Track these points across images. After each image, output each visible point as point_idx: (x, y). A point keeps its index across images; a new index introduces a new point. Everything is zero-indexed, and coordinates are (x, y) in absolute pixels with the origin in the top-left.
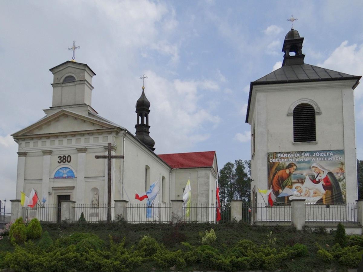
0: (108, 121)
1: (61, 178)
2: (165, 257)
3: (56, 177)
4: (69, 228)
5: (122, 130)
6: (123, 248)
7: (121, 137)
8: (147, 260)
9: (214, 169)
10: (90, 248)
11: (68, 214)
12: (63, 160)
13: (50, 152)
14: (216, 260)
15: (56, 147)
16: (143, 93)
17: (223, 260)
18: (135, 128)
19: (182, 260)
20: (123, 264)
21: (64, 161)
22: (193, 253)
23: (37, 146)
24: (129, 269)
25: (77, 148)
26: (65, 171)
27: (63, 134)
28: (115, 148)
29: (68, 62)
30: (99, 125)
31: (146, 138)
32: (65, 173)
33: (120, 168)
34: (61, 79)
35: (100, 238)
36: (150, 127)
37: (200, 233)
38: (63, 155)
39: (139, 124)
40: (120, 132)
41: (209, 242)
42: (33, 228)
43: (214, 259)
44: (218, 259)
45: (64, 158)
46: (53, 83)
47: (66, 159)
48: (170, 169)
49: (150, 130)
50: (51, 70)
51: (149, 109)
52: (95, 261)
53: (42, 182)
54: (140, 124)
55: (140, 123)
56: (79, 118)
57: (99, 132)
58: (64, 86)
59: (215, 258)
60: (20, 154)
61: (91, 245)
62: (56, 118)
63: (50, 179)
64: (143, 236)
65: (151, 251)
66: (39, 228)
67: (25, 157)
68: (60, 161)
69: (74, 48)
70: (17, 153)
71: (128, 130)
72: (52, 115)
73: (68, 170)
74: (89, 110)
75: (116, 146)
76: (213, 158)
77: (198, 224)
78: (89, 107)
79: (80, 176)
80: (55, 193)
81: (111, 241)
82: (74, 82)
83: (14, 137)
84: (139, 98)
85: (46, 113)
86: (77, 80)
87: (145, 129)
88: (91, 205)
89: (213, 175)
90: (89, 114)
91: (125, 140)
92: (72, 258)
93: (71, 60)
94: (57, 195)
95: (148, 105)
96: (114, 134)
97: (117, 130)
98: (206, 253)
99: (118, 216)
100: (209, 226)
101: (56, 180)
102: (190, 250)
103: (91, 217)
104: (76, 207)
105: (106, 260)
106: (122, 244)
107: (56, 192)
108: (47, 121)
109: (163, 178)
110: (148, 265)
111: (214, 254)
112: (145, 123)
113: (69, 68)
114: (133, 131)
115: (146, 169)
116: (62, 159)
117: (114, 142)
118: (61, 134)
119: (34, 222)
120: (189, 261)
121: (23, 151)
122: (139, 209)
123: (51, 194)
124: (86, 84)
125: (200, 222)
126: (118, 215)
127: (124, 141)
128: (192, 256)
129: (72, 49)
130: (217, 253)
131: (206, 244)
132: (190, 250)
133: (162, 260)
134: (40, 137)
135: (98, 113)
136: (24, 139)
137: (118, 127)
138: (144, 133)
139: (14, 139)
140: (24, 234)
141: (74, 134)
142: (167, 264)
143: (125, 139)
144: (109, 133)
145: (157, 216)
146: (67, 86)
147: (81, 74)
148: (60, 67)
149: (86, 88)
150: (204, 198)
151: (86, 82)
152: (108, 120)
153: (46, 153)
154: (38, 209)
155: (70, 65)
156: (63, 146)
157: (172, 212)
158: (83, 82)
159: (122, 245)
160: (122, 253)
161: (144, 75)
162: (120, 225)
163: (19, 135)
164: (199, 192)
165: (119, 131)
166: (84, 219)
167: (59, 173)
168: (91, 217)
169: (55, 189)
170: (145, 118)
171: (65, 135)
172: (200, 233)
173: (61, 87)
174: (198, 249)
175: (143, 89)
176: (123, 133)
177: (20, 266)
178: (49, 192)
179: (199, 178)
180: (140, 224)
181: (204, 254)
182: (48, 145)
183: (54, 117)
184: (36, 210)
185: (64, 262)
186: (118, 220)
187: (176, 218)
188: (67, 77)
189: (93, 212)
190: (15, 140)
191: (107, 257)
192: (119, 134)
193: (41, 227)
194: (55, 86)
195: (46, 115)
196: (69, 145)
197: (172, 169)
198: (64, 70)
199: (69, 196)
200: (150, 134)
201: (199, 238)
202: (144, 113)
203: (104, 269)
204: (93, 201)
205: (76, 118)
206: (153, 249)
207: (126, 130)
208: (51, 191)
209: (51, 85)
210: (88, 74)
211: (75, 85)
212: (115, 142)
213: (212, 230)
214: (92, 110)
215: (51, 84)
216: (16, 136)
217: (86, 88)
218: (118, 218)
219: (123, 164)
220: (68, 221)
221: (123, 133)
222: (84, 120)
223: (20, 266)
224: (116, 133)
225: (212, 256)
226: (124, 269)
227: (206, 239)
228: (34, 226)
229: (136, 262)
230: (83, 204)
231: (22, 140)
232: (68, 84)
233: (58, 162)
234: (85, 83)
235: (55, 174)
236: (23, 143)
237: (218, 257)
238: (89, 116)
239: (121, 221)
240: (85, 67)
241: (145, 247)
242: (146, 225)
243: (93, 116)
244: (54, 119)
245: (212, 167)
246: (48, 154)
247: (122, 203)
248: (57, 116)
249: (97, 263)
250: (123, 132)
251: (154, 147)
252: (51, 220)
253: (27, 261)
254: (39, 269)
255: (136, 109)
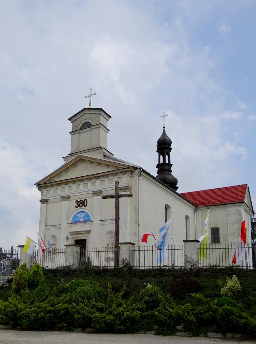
0: (123, 162)
1: (78, 222)
2: (170, 311)
3: (73, 222)
4: (72, 274)
5: (136, 168)
6: (121, 299)
7: (136, 176)
8: (148, 315)
9: (247, 204)
10: (83, 298)
11: (72, 258)
12: (80, 204)
13: (68, 198)
14: (238, 319)
15: (74, 192)
16: (164, 132)
17: (249, 318)
18: (156, 167)
19: (192, 318)
20: (118, 319)
21: (81, 205)
22: (207, 308)
23: (57, 193)
24: (124, 326)
25: (92, 191)
26: (82, 215)
27: (80, 179)
28: (130, 188)
29: (85, 109)
30: (113, 166)
31: (168, 176)
32: (81, 217)
33: (135, 209)
34: (78, 127)
35: (100, 286)
36: (172, 165)
37: (220, 282)
38: (84, 199)
39: (161, 163)
40: (135, 171)
41: (230, 292)
42: (34, 274)
43: (234, 317)
44: (241, 317)
45: (81, 202)
46: (71, 131)
47: (83, 203)
48: (194, 208)
49: (172, 169)
50: (69, 119)
51: (171, 147)
52: (85, 315)
53: (60, 227)
54: (162, 163)
55: (162, 162)
56: (94, 162)
57: (114, 174)
58: (81, 133)
59: (237, 316)
60: (42, 201)
61: (85, 294)
62: (73, 164)
63: (67, 224)
64: (147, 284)
65: (153, 304)
66: (40, 274)
67: (46, 204)
68: (77, 206)
69: (91, 95)
70: (40, 200)
71: (142, 168)
72: (70, 161)
73: (84, 214)
74: (104, 153)
75: (131, 186)
76: (245, 192)
77: (218, 269)
78: (104, 149)
79: (96, 219)
80: (72, 238)
81: (109, 290)
82: (90, 127)
83: (37, 185)
84: (160, 137)
85: (65, 161)
86: (92, 125)
87: (167, 167)
88: (107, 248)
89: (247, 211)
90: (105, 156)
91: (140, 179)
92: (62, 311)
93: (87, 107)
94: (74, 240)
95: (170, 143)
96: (129, 174)
97: (132, 170)
98: (223, 309)
99: (123, 261)
100: (233, 272)
101: (73, 225)
102: (203, 303)
103: (109, 262)
104: (57, 252)
105: (97, 314)
106: (121, 294)
107: (73, 237)
108: (65, 168)
109: (187, 217)
110: (148, 321)
111: (235, 309)
112: (167, 162)
113: (86, 114)
114: (154, 172)
115: (166, 209)
116: (79, 203)
117: (128, 182)
118: (77, 179)
119: (35, 268)
120: (201, 318)
121: (45, 198)
122: (151, 251)
123: (69, 239)
124: (101, 128)
125: (220, 267)
126: (123, 260)
127: (140, 180)
128: (205, 312)
129: (89, 96)
130: (241, 308)
131: (226, 296)
132: (203, 303)
133: (165, 316)
134: (59, 184)
135: (114, 155)
136: (46, 187)
137: (132, 166)
138: (166, 172)
139: (38, 187)
140: (25, 281)
141: (90, 178)
142: (173, 322)
143: (140, 177)
144: (123, 173)
145: (170, 260)
146: (84, 132)
147: (97, 119)
148: (78, 115)
149: (102, 131)
150: (236, 238)
151: (101, 126)
152: (122, 160)
153: (64, 198)
154: (57, 254)
155: (86, 112)
156: (79, 190)
157: (185, 255)
158: (98, 126)
159: (121, 296)
160: (120, 305)
161: (164, 113)
162: (125, 271)
163: (41, 183)
164: (230, 231)
165: (133, 171)
166: (91, 264)
167: (76, 218)
168: (106, 262)
169: (72, 233)
170: (167, 156)
171: (81, 179)
172: (220, 282)
173: (78, 134)
174: (214, 304)
175: (164, 128)
176: (138, 172)
177: (9, 317)
178: (67, 237)
179: (229, 215)
180: (148, 270)
181: (221, 310)
182: (66, 190)
183: (72, 163)
184: (56, 255)
185: (52, 315)
186: (123, 266)
187: (189, 262)
188: (84, 124)
189: (109, 256)
190: (38, 189)
191: (101, 310)
192: (134, 173)
193: (42, 274)
194: (73, 133)
195: (65, 162)
196: (85, 189)
197: (196, 207)
198: (81, 117)
199: (85, 240)
200: (172, 173)
201: (217, 287)
202: (166, 151)
203: (95, 325)
204: (108, 245)
205: (92, 161)
206: (156, 300)
207: (141, 169)
208: (69, 235)
209: (70, 134)
210: (103, 117)
211: (91, 130)
212: (130, 182)
213: (235, 276)
214: (108, 152)
215: (70, 132)
216: (40, 185)
217: (102, 131)
218: (123, 263)
219: (139, 204)
220: (72, 267)
221: (138, 172)
222: (99, 163)
223: (9, 317)
224: (131, 172)
225: (233, 314)
226: (118, 325)
227: (227, 289)
228: (35, 272)
229: (133, 318)
230: (102, 248)
231: (44, 188)
232: (85, 130)
233: (76, 206)
234: (99, 127)
235: (73, 219)
236: (45, 191)
237: (242, 315)
238: (104, 158)
239: (126, 266)
240: (100, 111)
241: (146, 298)
242: (154, 270)
243: (108, 157)
244: (72, 165)
245: (244, 202)
246: (67, 199)
247: (128, 245)
248: (74, 162)
249: (87, 317)
250: (138, 170)
251: (177, 186)
252: (42, 265)
253: (15, 312)
254: (25, 322)
255: (157, 148)
